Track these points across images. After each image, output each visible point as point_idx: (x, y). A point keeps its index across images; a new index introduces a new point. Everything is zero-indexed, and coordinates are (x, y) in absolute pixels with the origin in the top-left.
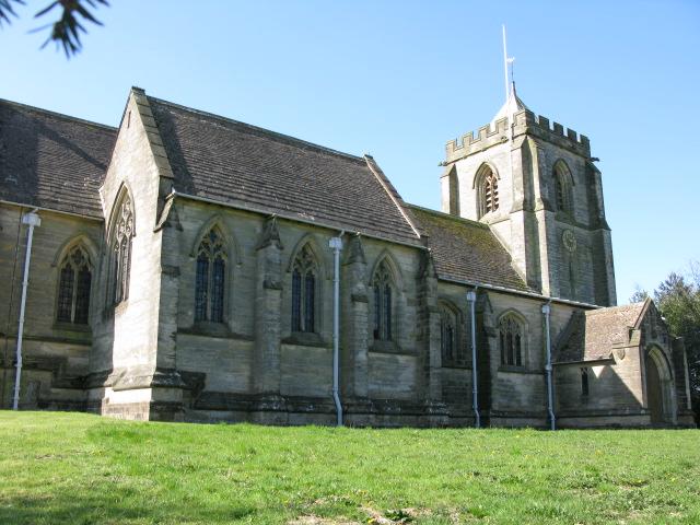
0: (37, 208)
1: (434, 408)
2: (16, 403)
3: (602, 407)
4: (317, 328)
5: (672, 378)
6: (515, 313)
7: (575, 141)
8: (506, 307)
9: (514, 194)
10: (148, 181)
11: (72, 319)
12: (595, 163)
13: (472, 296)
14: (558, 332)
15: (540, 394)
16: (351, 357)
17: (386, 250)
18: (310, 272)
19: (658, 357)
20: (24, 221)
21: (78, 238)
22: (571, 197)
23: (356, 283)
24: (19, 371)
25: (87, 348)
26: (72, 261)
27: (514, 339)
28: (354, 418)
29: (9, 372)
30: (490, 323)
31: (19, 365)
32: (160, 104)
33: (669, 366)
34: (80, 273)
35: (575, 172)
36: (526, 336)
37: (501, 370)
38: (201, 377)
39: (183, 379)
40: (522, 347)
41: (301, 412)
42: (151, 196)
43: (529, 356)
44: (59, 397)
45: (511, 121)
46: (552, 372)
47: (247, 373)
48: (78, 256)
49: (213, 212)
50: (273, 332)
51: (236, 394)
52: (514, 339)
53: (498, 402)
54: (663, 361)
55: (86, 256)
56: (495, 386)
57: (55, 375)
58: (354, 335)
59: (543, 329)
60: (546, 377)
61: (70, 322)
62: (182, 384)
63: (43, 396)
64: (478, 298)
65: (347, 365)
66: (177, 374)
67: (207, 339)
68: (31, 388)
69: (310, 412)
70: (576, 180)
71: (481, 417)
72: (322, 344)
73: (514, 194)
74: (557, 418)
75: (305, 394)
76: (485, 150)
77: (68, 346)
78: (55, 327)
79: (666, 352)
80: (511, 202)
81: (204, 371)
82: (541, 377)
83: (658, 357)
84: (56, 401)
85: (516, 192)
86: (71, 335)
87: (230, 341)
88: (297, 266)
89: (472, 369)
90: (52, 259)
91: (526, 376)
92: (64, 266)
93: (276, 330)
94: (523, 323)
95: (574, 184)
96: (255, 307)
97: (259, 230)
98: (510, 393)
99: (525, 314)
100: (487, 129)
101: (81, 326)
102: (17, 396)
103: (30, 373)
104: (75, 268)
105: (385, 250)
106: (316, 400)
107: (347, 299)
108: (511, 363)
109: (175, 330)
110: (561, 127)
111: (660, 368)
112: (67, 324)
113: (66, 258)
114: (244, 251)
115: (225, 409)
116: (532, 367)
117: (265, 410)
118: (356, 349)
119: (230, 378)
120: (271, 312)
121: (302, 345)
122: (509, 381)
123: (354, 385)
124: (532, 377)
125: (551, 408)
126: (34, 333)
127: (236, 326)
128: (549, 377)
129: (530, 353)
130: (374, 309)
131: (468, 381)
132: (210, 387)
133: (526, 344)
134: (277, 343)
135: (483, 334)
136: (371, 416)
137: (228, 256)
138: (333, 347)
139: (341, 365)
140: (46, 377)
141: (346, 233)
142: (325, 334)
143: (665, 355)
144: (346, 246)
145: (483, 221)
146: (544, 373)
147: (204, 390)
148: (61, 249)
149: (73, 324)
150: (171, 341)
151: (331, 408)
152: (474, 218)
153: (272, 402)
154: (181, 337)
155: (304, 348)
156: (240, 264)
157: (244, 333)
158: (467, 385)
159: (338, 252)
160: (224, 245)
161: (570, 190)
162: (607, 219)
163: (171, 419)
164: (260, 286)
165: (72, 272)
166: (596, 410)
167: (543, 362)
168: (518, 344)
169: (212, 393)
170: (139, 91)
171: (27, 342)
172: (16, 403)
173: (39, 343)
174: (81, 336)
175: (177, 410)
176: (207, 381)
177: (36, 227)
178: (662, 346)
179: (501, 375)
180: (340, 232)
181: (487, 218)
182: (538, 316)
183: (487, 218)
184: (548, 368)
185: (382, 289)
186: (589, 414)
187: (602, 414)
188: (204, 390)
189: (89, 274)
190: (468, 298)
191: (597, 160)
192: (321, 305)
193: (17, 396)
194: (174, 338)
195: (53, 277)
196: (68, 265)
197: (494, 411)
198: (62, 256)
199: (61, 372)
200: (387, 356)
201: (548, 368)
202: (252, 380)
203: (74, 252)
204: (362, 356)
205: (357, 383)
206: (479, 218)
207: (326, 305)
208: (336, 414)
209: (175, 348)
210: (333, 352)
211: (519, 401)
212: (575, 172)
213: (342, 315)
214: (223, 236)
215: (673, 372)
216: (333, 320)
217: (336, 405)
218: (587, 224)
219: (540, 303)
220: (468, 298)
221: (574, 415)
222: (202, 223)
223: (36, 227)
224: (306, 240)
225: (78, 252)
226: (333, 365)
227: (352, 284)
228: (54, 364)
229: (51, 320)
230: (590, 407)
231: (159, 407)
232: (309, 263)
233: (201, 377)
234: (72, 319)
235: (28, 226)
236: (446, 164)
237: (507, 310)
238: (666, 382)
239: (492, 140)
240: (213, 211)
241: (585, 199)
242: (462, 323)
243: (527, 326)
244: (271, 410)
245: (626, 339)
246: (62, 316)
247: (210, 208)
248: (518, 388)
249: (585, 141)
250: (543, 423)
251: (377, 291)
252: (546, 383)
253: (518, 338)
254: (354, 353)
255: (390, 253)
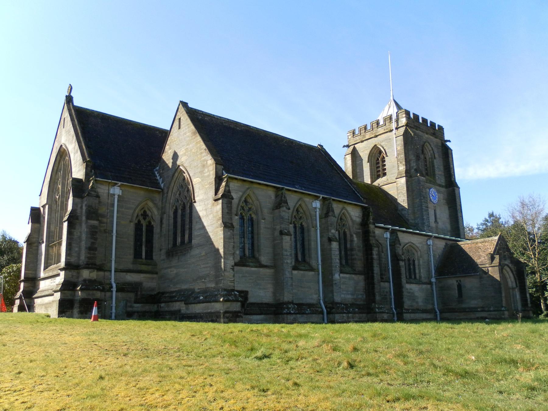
0: (120, 183)
1: (378, 308)
2: (113, 315)
3: (472, 306)
4: (307, 259)
5: (517, 286)
6: (412, 245)
7: (435, 129)
8: (407, 241)
9: (398, 166)
10: (204, 166)
11: (144, 256)
12: (448, 143)
13: (388, 235)
14: (438, 256)
15: (429, 297)
16: (330, 277)
17: (344, 208)
18: (344, 230)
19: (508, 272)
20: (111, 191)
21: (144, 203)
22: (433, 166)
23: (331, 230)
24: (114, 293)
25: (155, 276)
26: (141, 218)
27: (411, 262)
28: (337, 316)
29: (108, 294)
30: (399, 251)
31: (114, 289)
32: (198, 113)
33: (515, 279)
34: (147, 226)
35: (436, 150)
36: (419, 260)
37: (407, 283)
38: (246, 293)
39: (240, 296)
40: (417, 267)
41: (303, 314)
42: (209, 176)
43: (422, 273)
44: (139, 309)
45: (394, 117)
46: (435, 283)
47: (271, 290)
48: (145, 215)
49: (247, 187)
50: (287, 263)
51: (266, 304)
52: (411, 262)
53: (407, 303)
54: (511, 275)
55: (150, 214)
56: (405, 293)
57: (136, 295)
58: (331, 263)
59: (429, 255)
60: (432, 287)
61: (141, 258)
62: (240, 299)
63: (129, 309)
64: (391, 236)
65: (328, 283)
66: (236, 293)
67: (248, 268)
68: (122, 304)
69: (308, 314)
70: (436, 156)
71: (397, 313)
72: (312, 269)
73: (398, 166)
74: (441, 313)
75: (304, 302)
76: (376, 136)
77: (142, 275)
78: (134, 263)
79: (513, 269)
80: (396, 171)
81: (247, 290)
82: (429, 286)
83: (508, 272)
84: (138, 312)
85: (400, 165)
86: (144, 268)
87: (261, 269)
88: (242, 211)
89: (390, 282)
90: (130, 217)
91: (421, 286)
92: (137, 222)
93: (289, 261)
94: (417, 251)
95: (435, 158)
96: (274, 247)
97: (273, 197)
98: (413, 297)
99: (418, 245)
100: (378, 123)
101: (149, 261)
102: (114, 310)
103: (119, 294)
104: (144, 223)
105: (344, 208)
106: (310, 305)
107: (325, 239)
108: (411, 277)
109: (233, 264)
110: (427, 120)
111: (509, 280)
112: (140, 260)
113: (137, 216)
114: (265, 211)
115: (261, 314)
116: (424, 280)
117: (287, 314)
118: (333, 272)
119: (262, 293)
120: (286, 251)
121: (301, 270)
122: (411, 289)
123: (333, 295)
124: (424, 286)
125: (436, 307)
126: (121, 267)
127: (264, 259)
128: (434, 286)
129: (422, 271)
130: (293, 239)
131: (388, 290)
132: (251, 300)
133: (419, 265)
134: (290, 270)
135: (396, 258)
136: (344, 315)
137: (256, 214)
138: (318, 272)
139: (323, 282)
140: (132, 296)
141: (323, 197)
142: (313, 263)
143: (512, 272)
144: (323, 205)
145: (376, 183)
146: (430, 283)
147: (248, 302)
148: (135, 210)
149: (144, 261)
150: (231, 271)
151: (320, 310)
152: (369, 182)
153: (290, 308)
154: (236, 268)
155: (302, 272)
156: (264, 219)
157: (268, 264)
158: (387, 292)
159: (318, 210)
160: (253, 207)
161: (433, 163)
162: (457, 181)
163: (235, 322)
164: (277, 233)
165: (142, 225)
166: (469, 308)
167: (430, 277)
168: (414, 265)
169: (253, 304)
170: (184, 104)
171: (117, 273)
172: (113, 315)
173: (124, 274)
174: (149, 268)
175: (238, 316)
176: (250, 295)
177: (119, 196)
178: (510, 265)
179: (408, 286)
180: (319, 197)
181: (379, 182)
182: (425, 247)
183: (379, 182)
184: (433, 280)
185: (298, 225)
186: (464, 310)
187: (473, 310)
188: (248, 302)
189: (152, 227)
190: (385, 236)
191: (449, 141)
192: (309, 244)
193: (114, 310)
194: (233, 269)
195: (131, 230)
196: (139, 221)
197: (406, 309)
198: (135, 215)
199: (139, 293)
200: (347, 276)
201: (433, 280)
202: (274, 293)
203: (142, 212)
204: (337, 276)
205: (335, 294)
206: (373, 181)
207: (313, 243)
208: (323, 314)
209: (234, 276)
210: (319, 274)
211: (417, 303)
212: (436, 150)
213: (322, 250)
214: (253, 201)
215: (518, 283)
216: (317, 254)
217: (322, 308)
218: (444, 184)
219: (426, 238)
220: (385, 236)
221: (452, 311)
222: (241, 193)
223: (119, 196)
224: (248, 192)
225: (145, 212)
226: (318, 283)
227: (328, 230)
228: (134, 287)
229: (131, 257)
230: (464, 306)
231: (227, 315)
232: (301, 218)
233: (246, 293)
234: (144, 256)
235: (114, 195)
236: (348, 146)
237: (408, 243)
238: (513, 289)
239: (381, 130)
240: (247, 185)
241: (442, 168)
242: (383, 252)
243: (419, 253)
244: (290, 313)
245: (488, 261)
246: (137, 254)
247: (245, 183)
248: (416, 294)
249: (441, 128)
250: (429, 316)
251: (295, 227)
252: (433, 290)
253: (414, 261)
254: (332, 275)
255: (346, 210)
